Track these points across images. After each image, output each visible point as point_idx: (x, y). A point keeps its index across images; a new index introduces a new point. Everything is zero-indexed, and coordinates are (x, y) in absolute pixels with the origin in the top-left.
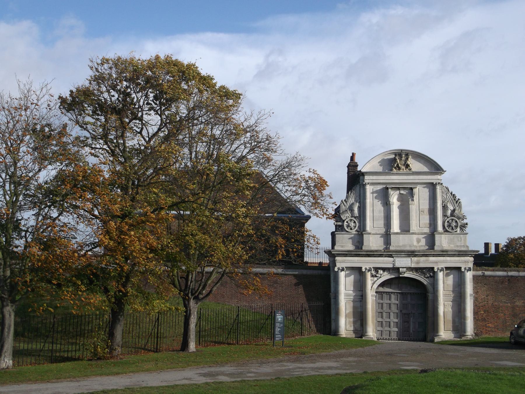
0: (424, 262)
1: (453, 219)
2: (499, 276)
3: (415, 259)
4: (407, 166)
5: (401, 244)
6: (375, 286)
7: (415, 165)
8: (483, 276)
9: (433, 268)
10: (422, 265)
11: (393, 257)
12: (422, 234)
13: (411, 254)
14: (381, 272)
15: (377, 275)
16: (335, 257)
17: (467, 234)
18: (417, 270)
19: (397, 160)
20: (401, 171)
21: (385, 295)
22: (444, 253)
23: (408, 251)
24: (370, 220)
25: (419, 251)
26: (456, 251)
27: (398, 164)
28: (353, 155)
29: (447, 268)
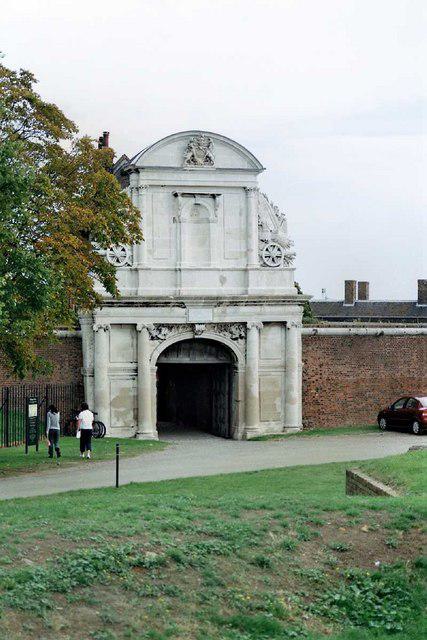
0: (232, 315)
2: (337, 336)
4: (208, 159)
6: (157, 355)
7: (221, 157)
9: (245, 324)
10: (228, 320)
13: (217, 302)
14: (165, 331)
15: (159, 336)
17: (294, 269)
18: (224, 327)
19: (198, 146)
28: (106, 135)
29: (266, 324)
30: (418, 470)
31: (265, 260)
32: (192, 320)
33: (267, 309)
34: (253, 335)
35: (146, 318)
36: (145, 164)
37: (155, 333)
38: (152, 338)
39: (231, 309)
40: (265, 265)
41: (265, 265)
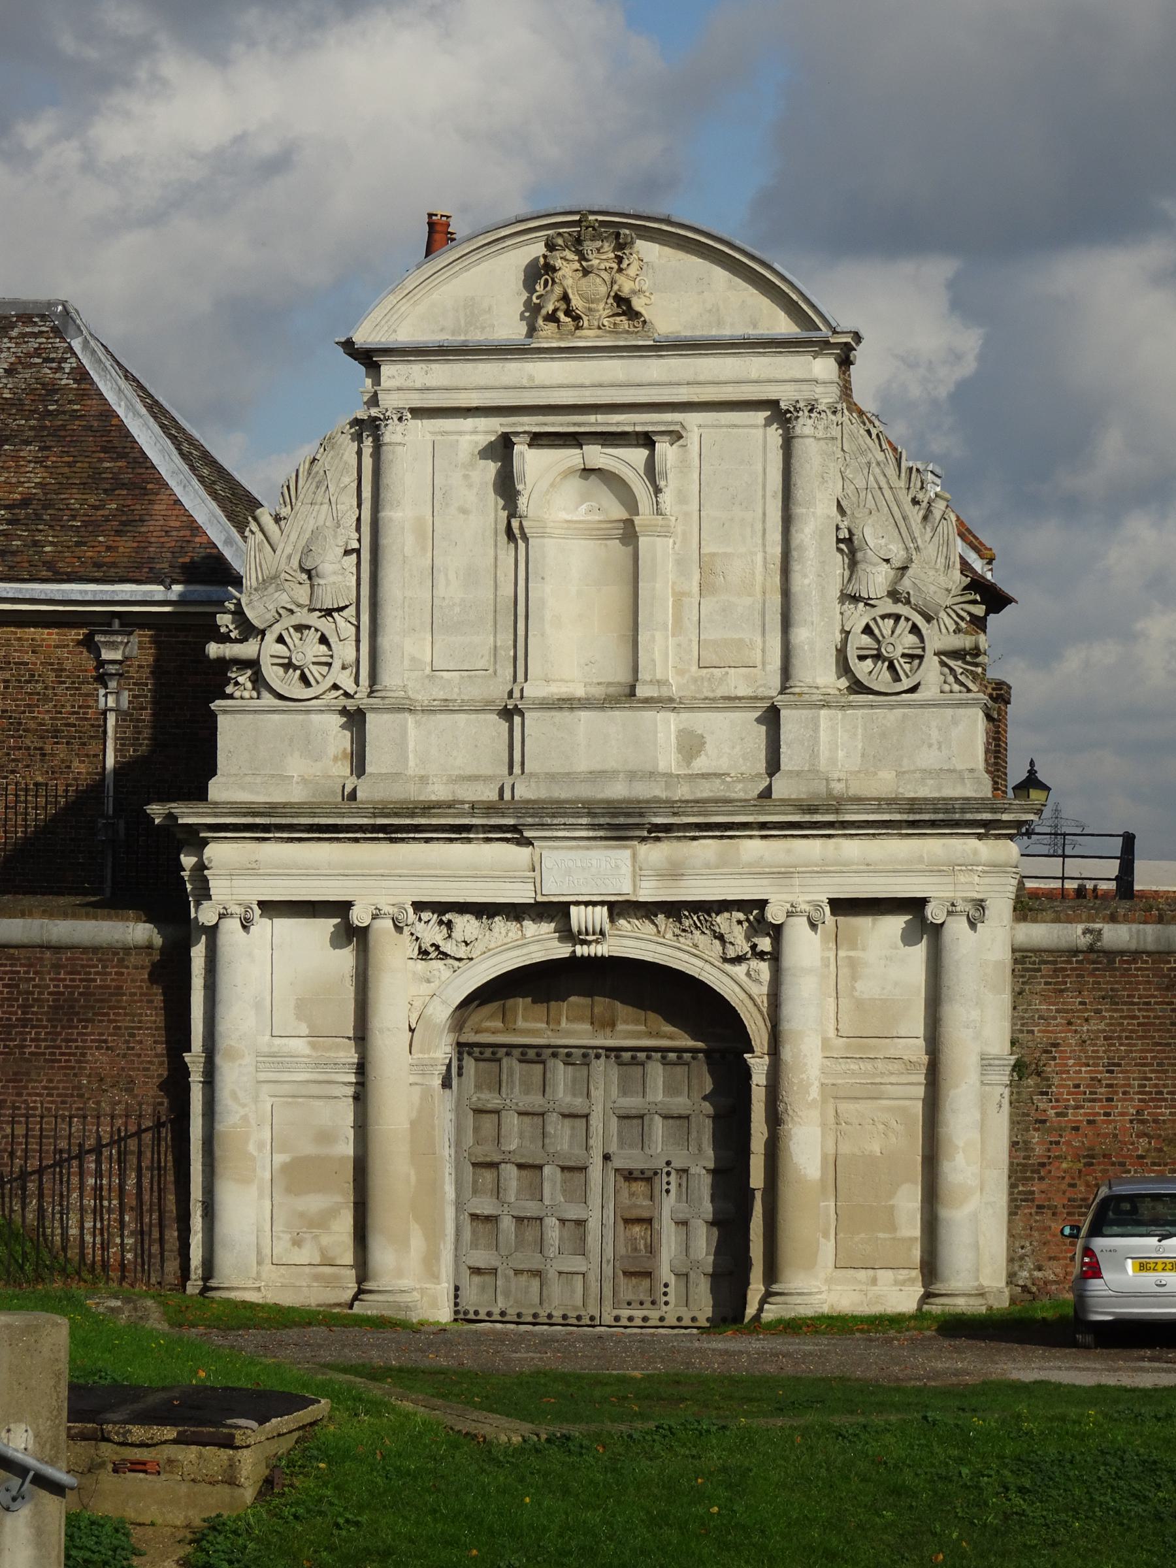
0: (709, 870)
1: (897, 618)
3: (655, 853)
5: (583, 764)
6: (442, 1012)
8: (1091, 949)
11: (528, 842)
12: (731, 702)
13: (750, 837)
14: (465, 925)
15: (447, 947)
16: (205, 842)
20: (588, 337)
21: (511, 1064)
22: (822, 817)
23: (614, 808)
24: (145, 592)
25: (674, 806)
26: (891, 803)
27: (565, 298)
29: (842, 906)
30: (143, 967)
31: (862, 669)
32: (554, 889)
33: (852, 848)
34: (805, 948)
35: (378, 878)
36: (404, 335)
37: (431, 933)
38: (423, 953)
39: (706, 849)
40: (858, 687)
41: (858, 687)
